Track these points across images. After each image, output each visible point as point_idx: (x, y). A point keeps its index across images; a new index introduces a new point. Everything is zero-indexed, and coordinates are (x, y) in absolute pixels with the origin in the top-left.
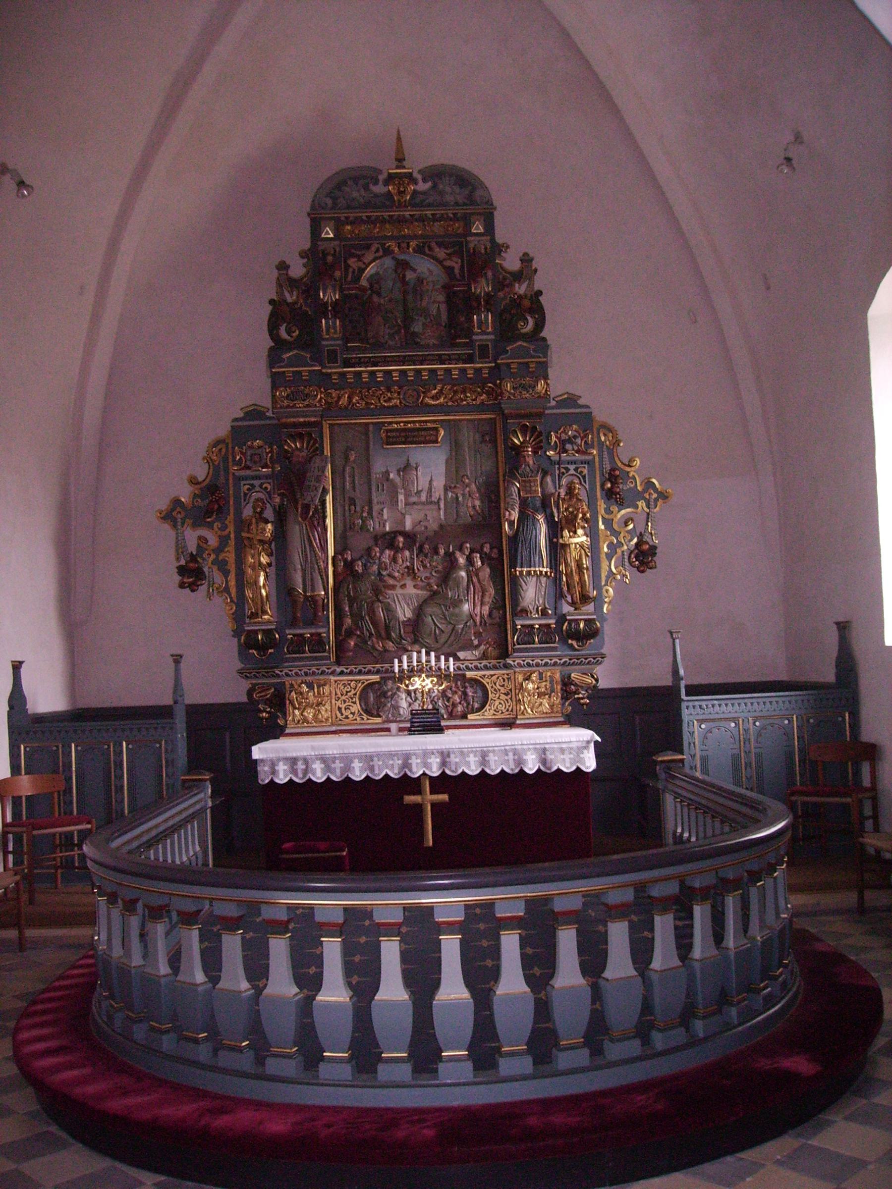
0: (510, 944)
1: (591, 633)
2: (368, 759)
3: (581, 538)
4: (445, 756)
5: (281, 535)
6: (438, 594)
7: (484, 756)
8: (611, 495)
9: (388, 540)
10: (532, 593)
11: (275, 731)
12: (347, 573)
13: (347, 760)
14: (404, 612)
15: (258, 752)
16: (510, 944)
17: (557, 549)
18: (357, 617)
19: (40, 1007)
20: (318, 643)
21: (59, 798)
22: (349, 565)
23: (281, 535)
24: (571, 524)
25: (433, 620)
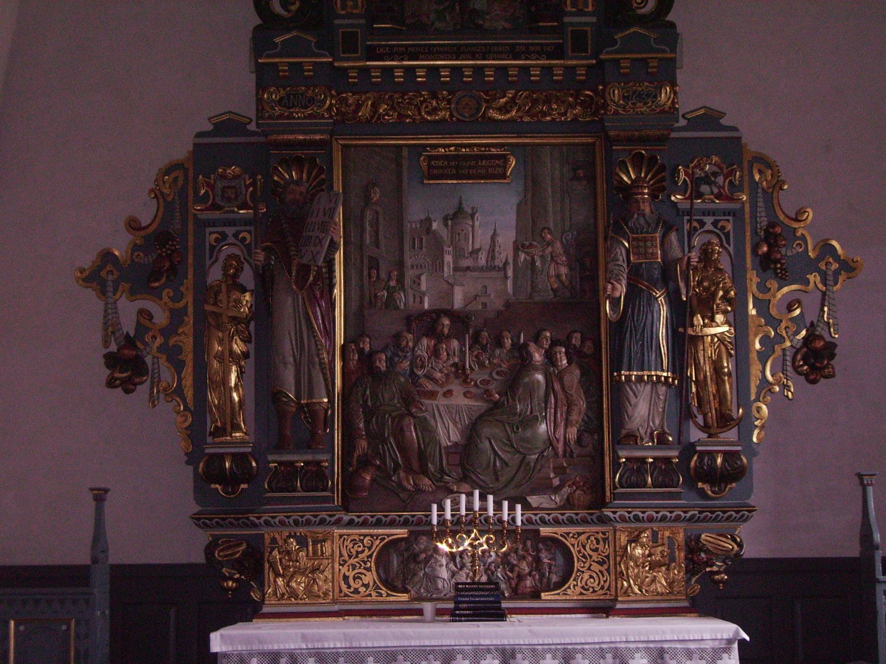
1: (733, 472)
5: (264, 310)
6: (502, 407)
9: (427, 323)
10: (644, 410)
11: (246, 610)
12: (363, 371)
14: (448, 433)
17: (683, 344)
22: (367, 359)
23: (264, 310)
25: (492, 443)
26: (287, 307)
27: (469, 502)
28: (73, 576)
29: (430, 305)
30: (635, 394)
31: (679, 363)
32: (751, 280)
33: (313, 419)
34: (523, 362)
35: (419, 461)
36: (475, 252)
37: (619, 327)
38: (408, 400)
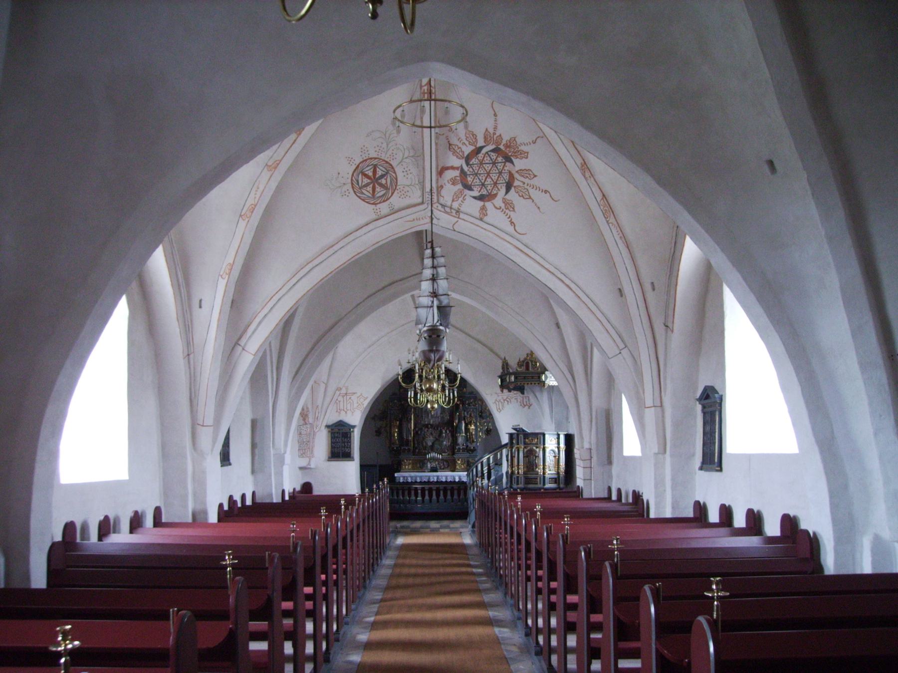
0: (442, 492)
1: (474, 450)
2: (421, 477)
3: (473, 427)
4: (438, 477)
5: (401, 425)
6: (439, 438)
7: (446, 477)
8: (481, 416)
9: (427, 426)
10: (460, 440)
11: (399, 471)
12: (416, 433)
13: (416, 477)
14: (430, 444)
15: (396, 475)
16: (442, 492)
17: (467, 430)
18: (418, 444)
19: (402, 581)
20: (409, 450)
21: (410, 566)
22: (417, 432)
23: (401, 425)
24: (470, 423)
25: (437, 446)
26: (404, 425)
27: (433, 455)
28: (375, 466)
29: (874, 563)
30: (270, 346)
31: (466, 433)
32: (281, 460)
33: (408, 441)
34: (441, 433)
35: (425, 448)
36: (373, 180)
37: (457, 426)
38: (424, 439)
